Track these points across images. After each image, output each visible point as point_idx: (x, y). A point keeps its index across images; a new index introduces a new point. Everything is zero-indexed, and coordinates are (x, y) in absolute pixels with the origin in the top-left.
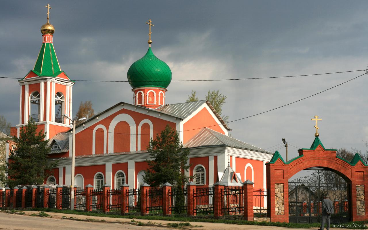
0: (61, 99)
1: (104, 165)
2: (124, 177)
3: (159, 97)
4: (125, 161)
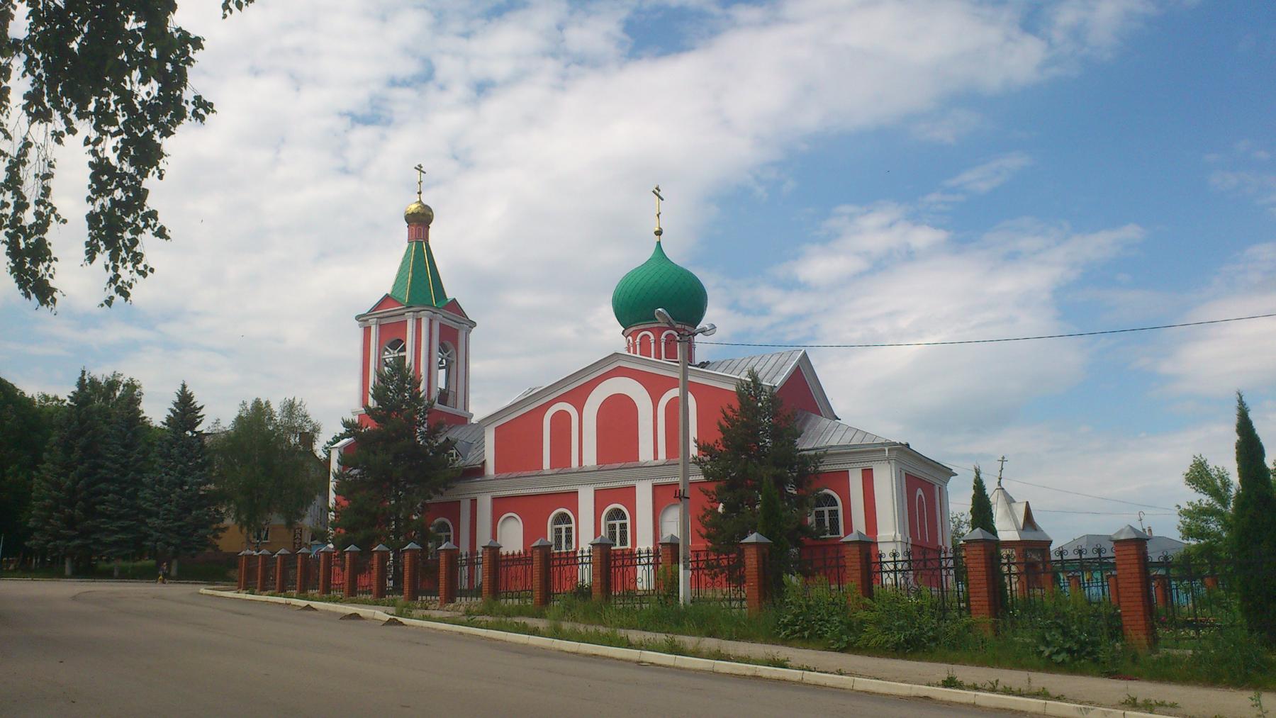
0: (448, 356)
1: (634, 487)
2: (626, 519)
3: (663, 345)
4: (575, 488)
